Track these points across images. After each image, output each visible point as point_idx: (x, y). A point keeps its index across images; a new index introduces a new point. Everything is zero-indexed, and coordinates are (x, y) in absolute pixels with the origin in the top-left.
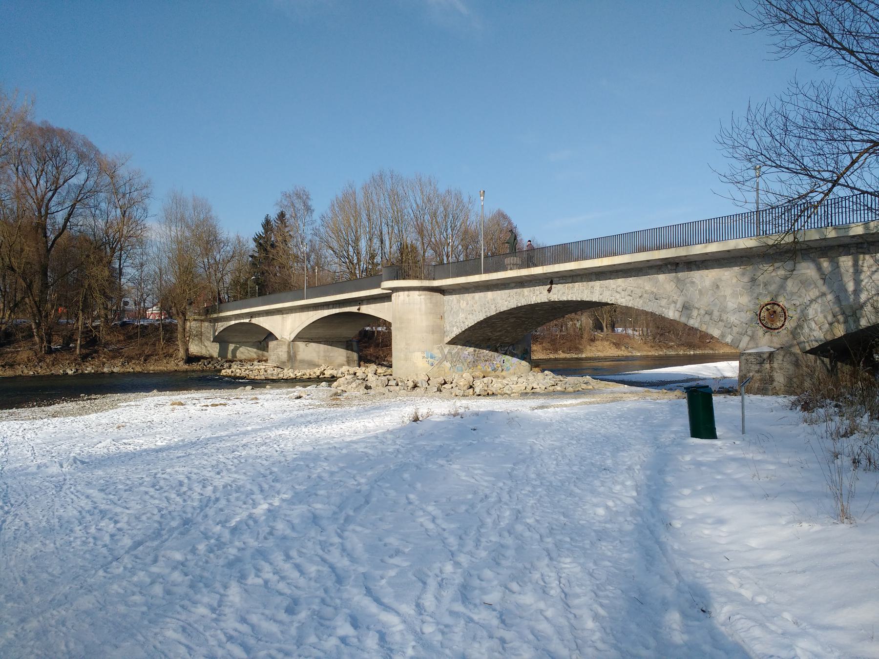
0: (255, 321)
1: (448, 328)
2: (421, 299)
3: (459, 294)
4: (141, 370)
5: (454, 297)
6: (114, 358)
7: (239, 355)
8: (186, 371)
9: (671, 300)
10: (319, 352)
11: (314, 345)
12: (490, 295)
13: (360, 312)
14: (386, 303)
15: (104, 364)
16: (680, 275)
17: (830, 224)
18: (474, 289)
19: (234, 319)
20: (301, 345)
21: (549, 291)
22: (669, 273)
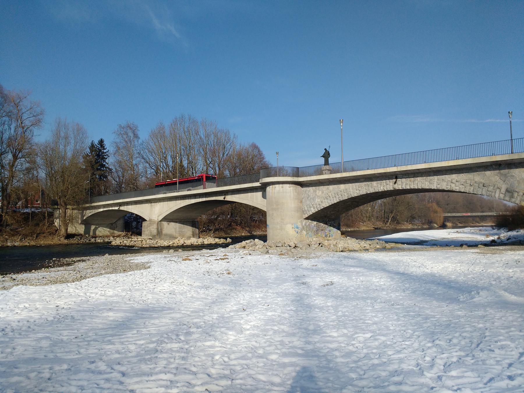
0: (122, 208)
1: (306, 209)
2: (290, 190)
3: (345, 184)
4: (35, 244)
5: (311, 188)
6: (13, 235)
7: (98, 233)
8: (67, 245)
9: (496, 187)
10: (176, 229)
11: (172, 224)
12: (342, 186)
13: (225, 200)
14: (249, 194)
15: (7, 240)
16: (502, 171)
17: (493, 154)
18: (328, 183)
19: (102, 207)
20: (165, 224)
21: (395, 183)
22: (494, 170)
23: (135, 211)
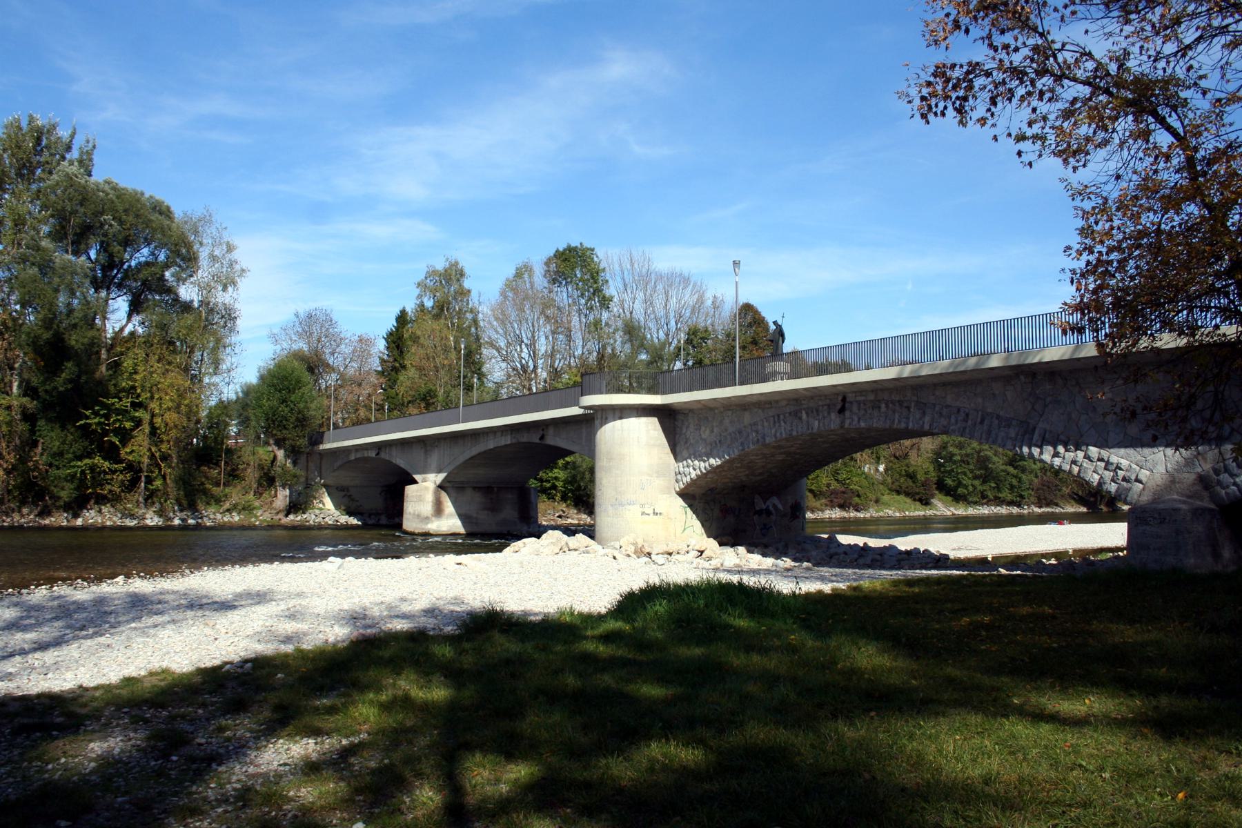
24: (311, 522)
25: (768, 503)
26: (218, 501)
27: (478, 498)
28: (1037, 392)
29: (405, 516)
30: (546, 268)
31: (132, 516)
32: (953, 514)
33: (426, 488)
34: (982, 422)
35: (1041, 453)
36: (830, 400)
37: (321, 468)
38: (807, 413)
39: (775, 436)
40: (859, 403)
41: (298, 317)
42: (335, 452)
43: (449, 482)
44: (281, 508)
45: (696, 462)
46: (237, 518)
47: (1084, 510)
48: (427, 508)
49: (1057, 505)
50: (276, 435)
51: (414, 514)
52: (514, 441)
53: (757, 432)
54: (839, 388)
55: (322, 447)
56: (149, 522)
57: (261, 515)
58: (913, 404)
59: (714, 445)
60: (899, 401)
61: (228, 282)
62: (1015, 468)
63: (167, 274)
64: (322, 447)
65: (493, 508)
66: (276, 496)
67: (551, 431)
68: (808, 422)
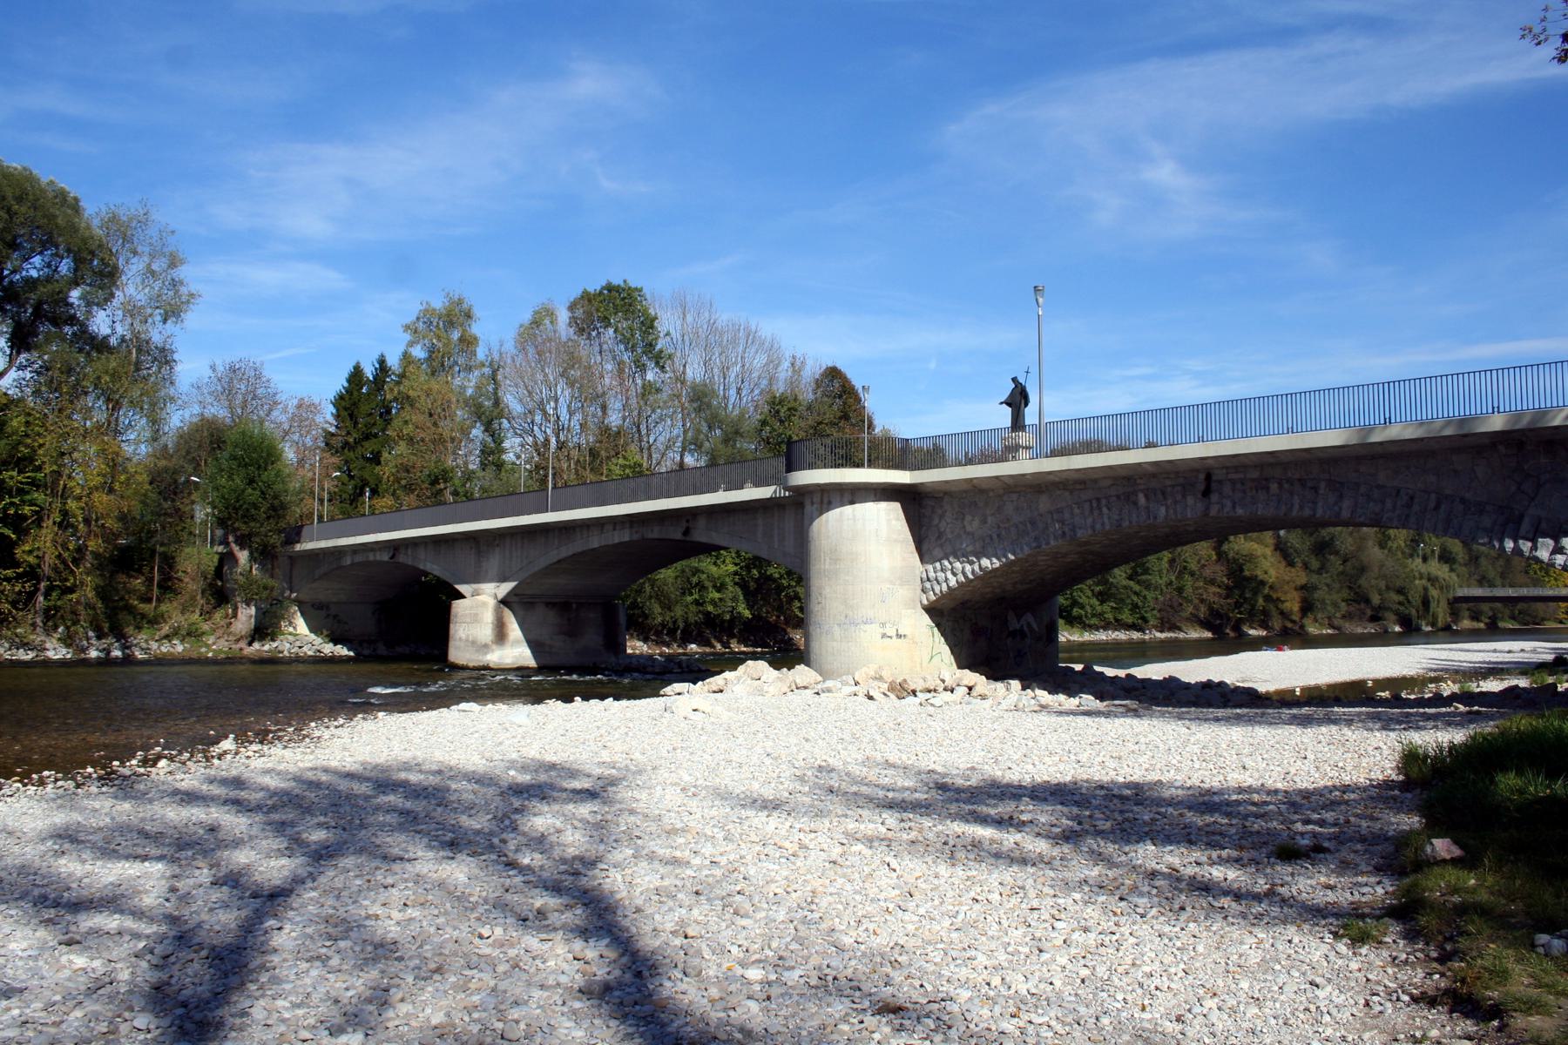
13: (688, 539)
17: (1496, 410)
23: (435, 567)
24: (286, 653)
25: (1023, 622)
26: (154, 621)
27: (552, 617)
28: (1526, 467)
29: (452, 644)
30: (570, 315)
31: (25, 645)
32: (1069, 641)
33: (484, 604)
34: (1437, 508)
35: (1535, 548)
36: (1185, 478)
37: (291, 578)
38: (1146, 497)
39: (1093, 527)
40: (1233, 482)
41: (214, 370)
42: (317, 555)
43: (516, 595)
44: (243, 633)
45: (958, 565)
46: (180, 648)
47: (1209, 635)
48: (485, 632)
49: (1180, 629)
50: (238, 529)
51: (467, 640)
52: (636, 537)
53: (1062, 522)
54: (1209, 461)
55: (298, 547)
56: (51, 654)
57: (214, 644)
58: (1323, 485)
59: (987, 540)
60: (1299, 480)
61: (172, 312)
62: (1138, 582)
63: (75, 295)
64: (298, 547)
65: (571, 630)
66: (235, 616)
67: (702, 522)
68: (1147, 508)
